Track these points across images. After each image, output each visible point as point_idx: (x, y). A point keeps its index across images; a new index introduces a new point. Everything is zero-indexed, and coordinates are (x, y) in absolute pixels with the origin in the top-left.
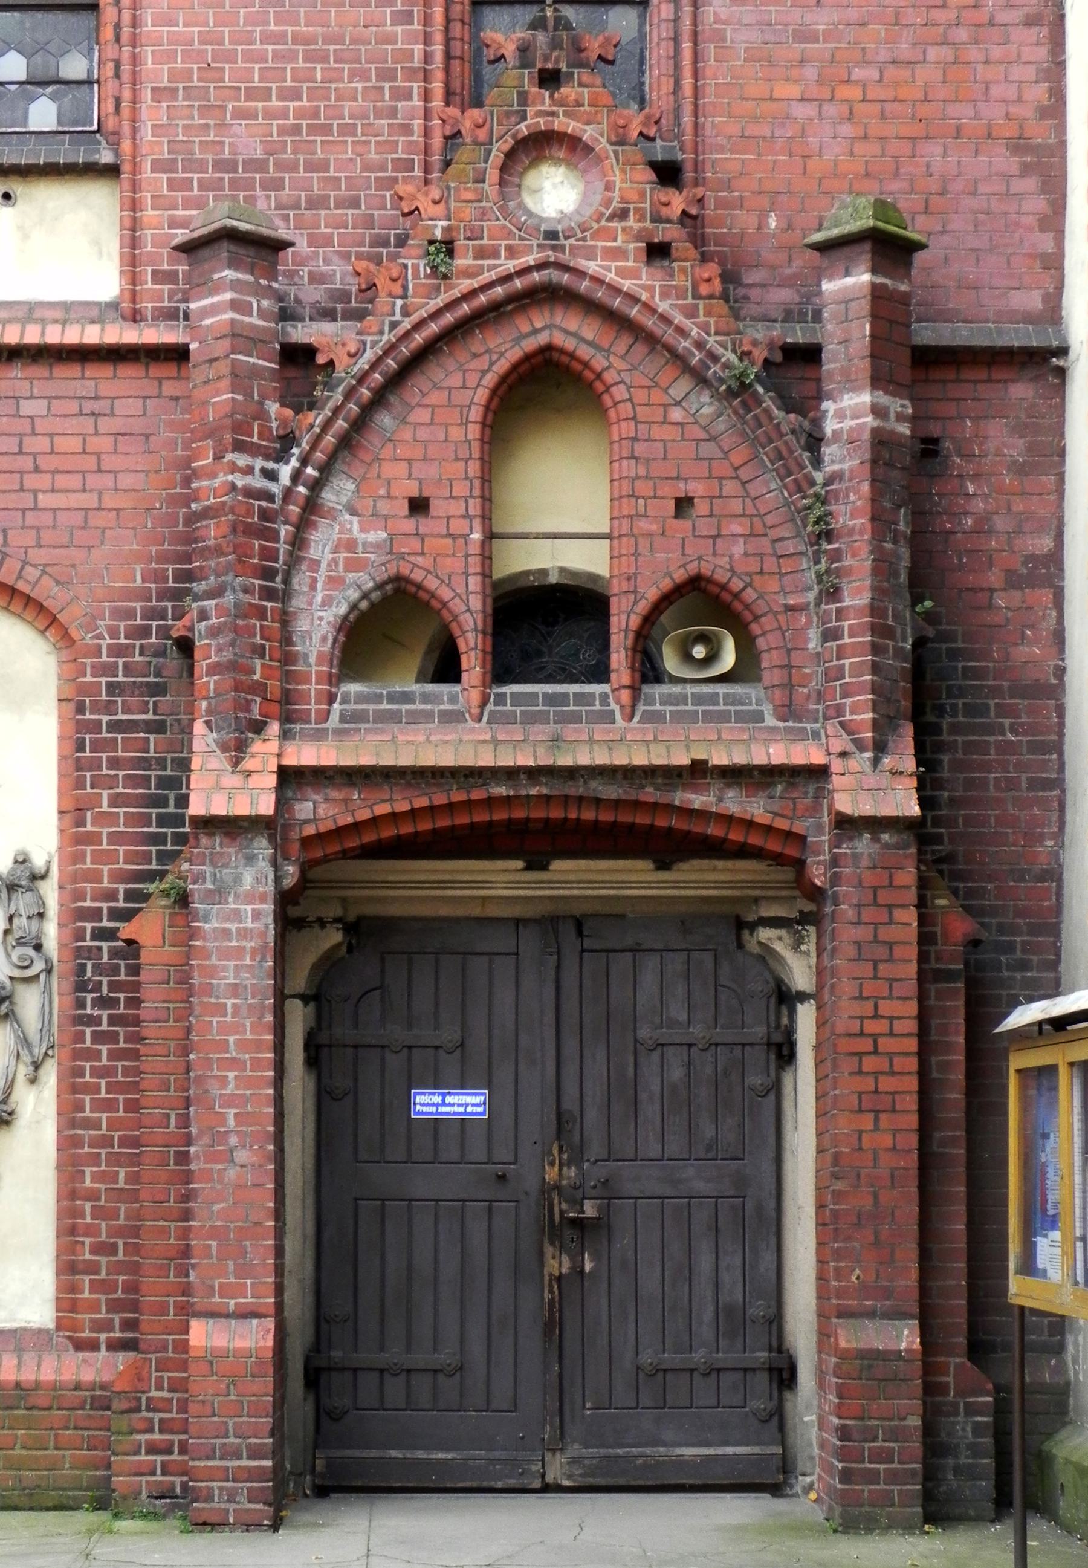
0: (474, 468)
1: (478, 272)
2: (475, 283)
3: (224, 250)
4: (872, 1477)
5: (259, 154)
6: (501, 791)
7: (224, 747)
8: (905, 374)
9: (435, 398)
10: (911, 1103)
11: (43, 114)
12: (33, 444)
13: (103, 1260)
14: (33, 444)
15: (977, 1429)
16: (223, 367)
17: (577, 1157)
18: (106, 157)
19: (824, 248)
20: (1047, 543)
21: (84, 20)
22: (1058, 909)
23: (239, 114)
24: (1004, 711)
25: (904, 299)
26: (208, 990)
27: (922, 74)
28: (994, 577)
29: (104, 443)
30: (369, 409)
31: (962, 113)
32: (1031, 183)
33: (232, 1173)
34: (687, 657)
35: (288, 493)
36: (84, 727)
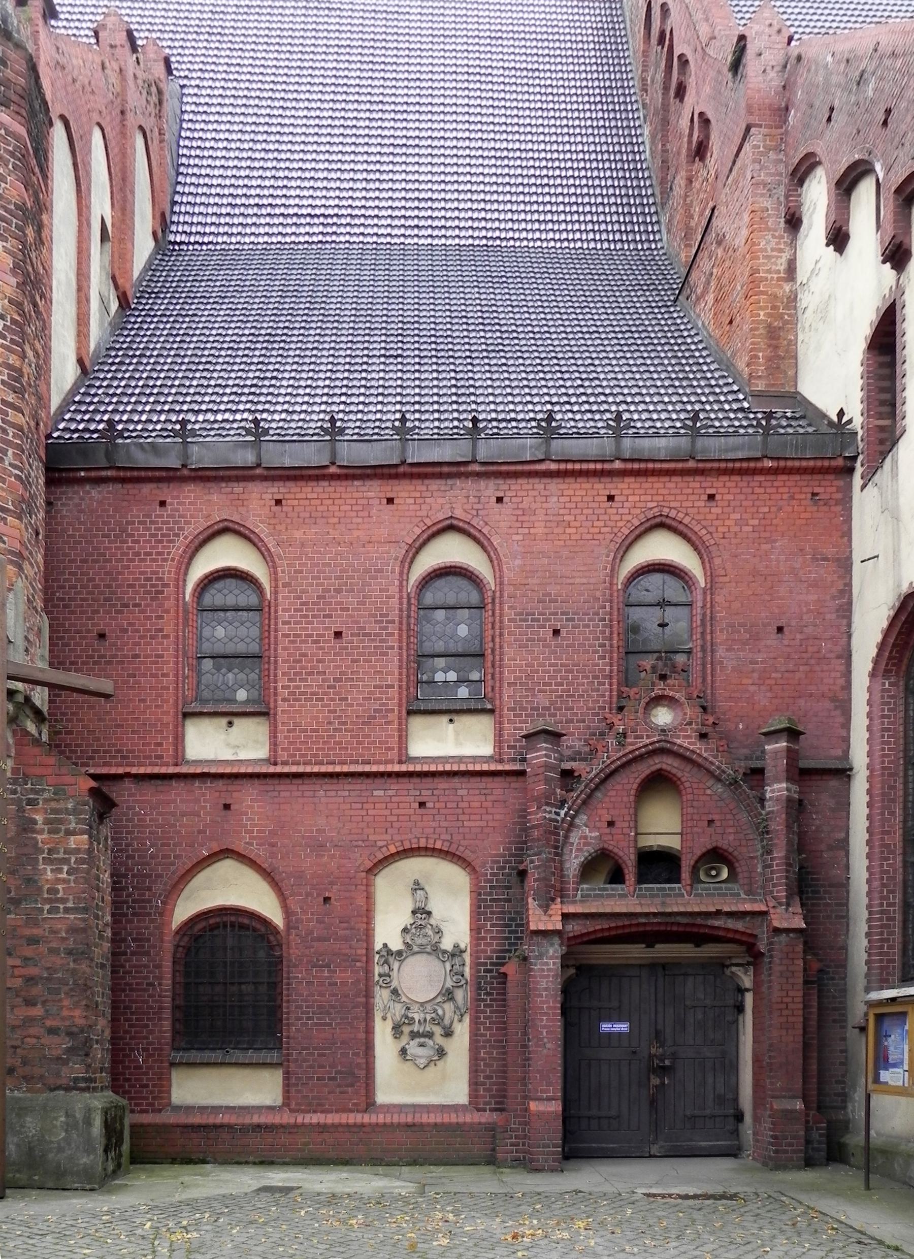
0: (632, 811)
1: (635, 744)
3: (543, 737)
4: (786, 1152)
6: (643, 920)
7: (540, 906)
8: (797, 777)
9: (618, 787)
10: (800, 1026)
11: (463, 692)
12: (461, 805)
14: (461, 805)
15: (821, 1135)
16: (541, 777)
17: (662, 1045)
18: (489, 707)
19: (765, 734)
20: (843, 835)
21: (480, 659)
22: (846, 960)
23: (540, 691)
24: (825, 892)
25: (797, 751)
26: (536, 989)
27: (798, 675)
28: (823, 847)
30: (593, 791)
31: (813, 689)
32: (838, 712)
34: (708, 875)
35: (563, 820)
36: (480, 900)
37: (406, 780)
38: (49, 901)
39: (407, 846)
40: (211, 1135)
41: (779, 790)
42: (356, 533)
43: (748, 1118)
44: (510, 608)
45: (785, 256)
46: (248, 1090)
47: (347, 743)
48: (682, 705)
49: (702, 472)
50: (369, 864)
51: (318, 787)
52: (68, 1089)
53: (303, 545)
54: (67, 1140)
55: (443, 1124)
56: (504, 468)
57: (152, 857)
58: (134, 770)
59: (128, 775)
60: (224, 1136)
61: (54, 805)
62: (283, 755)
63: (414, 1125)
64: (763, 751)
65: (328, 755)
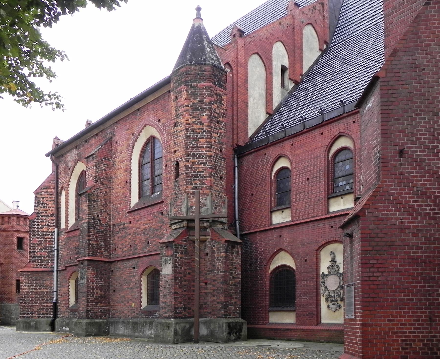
37: (327, 220)
38: (217, 270)
39: (328, 241)
40: (276, 331)
42: (312, 147)
46: (285, 319)
47: (311, 212)
50: (317, 248)
51: (303, 226)
52: (221, 317)
53: (298, 155)
54: (219, 330)
55: (337, 330)
57: (263, 253)
58: (258, 230)
59: (257, 232)
60: (279, 332)
61: (218, 246)
62: (294, 219)
63: (328, 330)
65: (305, 216)
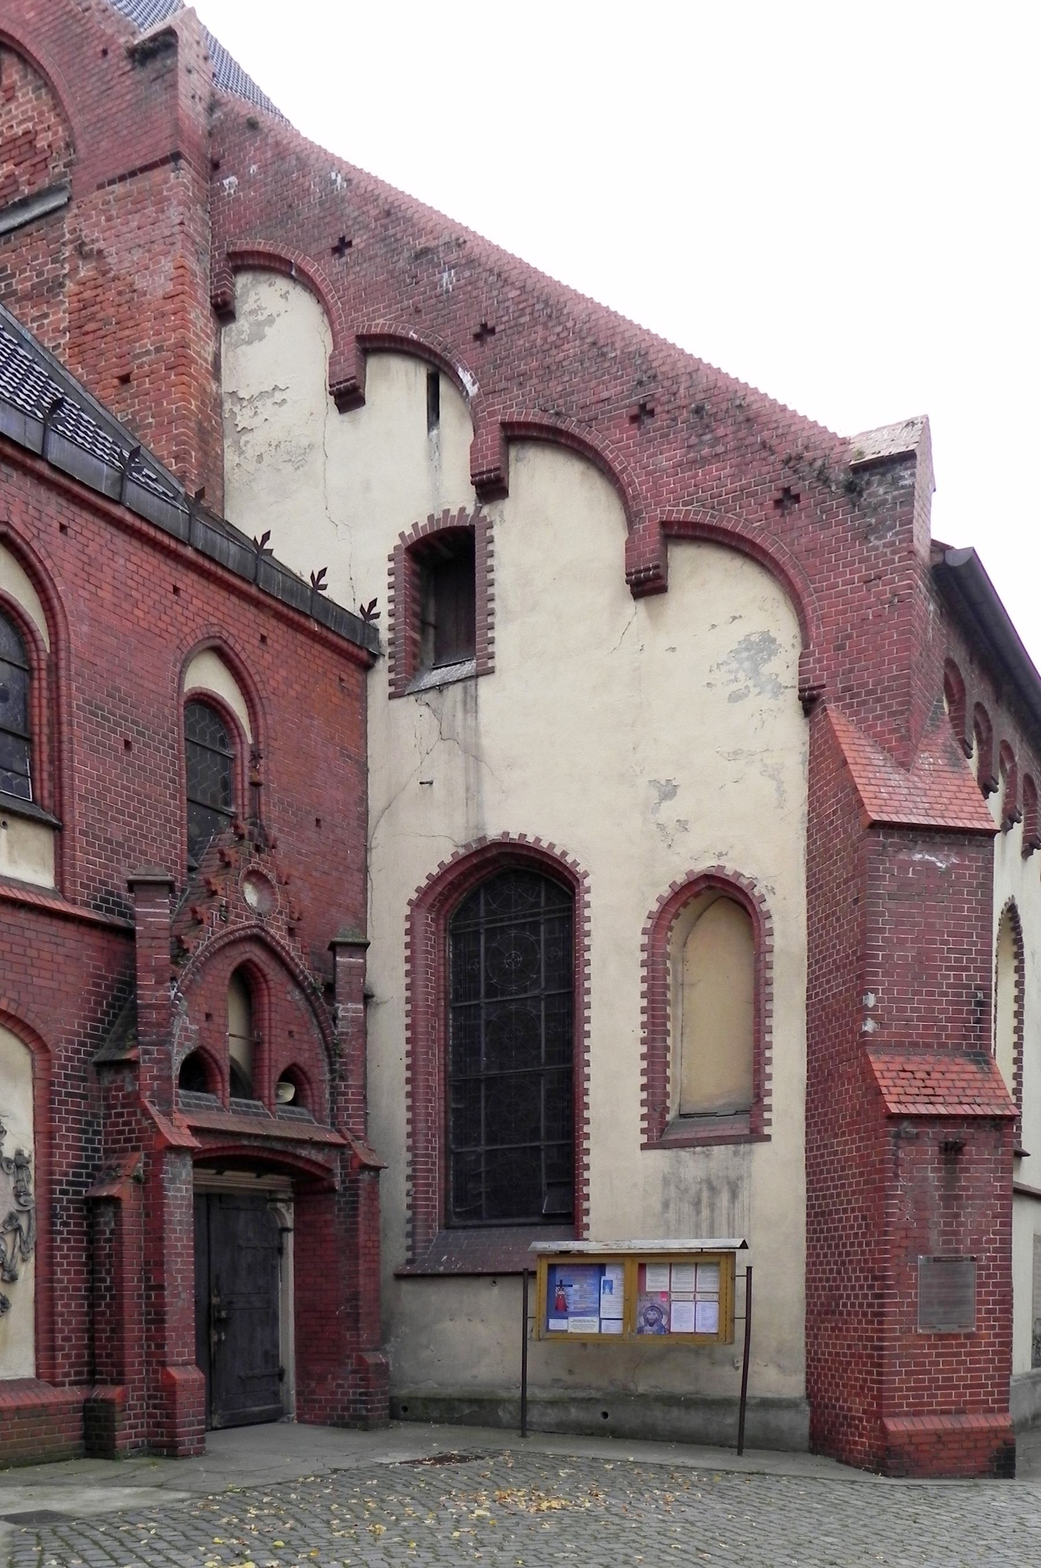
2: (235, 927)
5: (121, 840)
6: (245, 1142)
9: (214, 972)
13: (67, 1344)
23: (113, 818)
26: (170, 1222)
29: (60, 959)
33: (180, 1303)
41: (355, 1011)
43: (291, 1377)
44: (78, 689)
45: (211, 348)
48: (272, 887)
49: (257, 604)
56: (76, 488)
64: (335, 965)
